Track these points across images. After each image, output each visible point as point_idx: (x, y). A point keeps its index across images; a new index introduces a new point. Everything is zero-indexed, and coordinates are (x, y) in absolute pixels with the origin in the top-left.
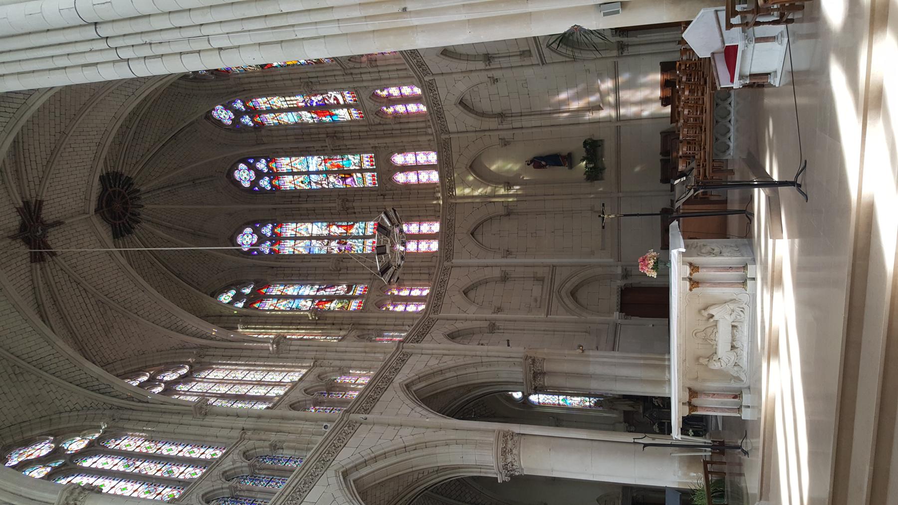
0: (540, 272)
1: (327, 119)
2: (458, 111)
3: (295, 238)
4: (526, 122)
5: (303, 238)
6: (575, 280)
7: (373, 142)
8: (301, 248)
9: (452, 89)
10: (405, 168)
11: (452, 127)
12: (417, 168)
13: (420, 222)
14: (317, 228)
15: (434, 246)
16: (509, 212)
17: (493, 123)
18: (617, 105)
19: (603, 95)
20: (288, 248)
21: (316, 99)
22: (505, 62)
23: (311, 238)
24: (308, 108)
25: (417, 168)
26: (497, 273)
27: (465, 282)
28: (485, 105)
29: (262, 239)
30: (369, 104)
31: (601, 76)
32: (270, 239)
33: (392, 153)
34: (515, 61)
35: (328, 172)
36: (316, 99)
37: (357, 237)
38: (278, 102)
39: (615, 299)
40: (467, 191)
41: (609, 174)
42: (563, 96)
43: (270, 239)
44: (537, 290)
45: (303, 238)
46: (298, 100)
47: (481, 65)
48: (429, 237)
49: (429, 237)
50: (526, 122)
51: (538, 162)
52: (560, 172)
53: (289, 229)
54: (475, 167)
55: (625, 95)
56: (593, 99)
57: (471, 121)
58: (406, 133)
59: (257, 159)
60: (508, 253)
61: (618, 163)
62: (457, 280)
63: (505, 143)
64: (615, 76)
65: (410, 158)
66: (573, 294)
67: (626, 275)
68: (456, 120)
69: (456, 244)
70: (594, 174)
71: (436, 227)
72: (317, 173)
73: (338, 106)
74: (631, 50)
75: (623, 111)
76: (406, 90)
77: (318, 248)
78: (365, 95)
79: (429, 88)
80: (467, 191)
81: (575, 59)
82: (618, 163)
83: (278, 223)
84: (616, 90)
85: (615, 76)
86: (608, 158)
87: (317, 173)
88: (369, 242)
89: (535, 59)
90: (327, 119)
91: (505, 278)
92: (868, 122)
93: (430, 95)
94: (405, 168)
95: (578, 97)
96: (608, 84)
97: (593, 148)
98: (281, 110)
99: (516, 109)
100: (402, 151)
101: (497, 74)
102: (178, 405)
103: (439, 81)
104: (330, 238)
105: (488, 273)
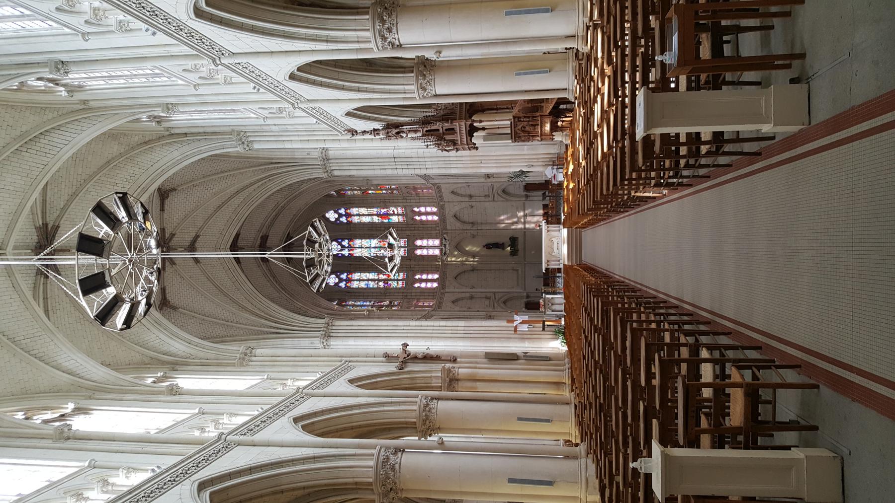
0: (489, 295)
1: (386, 221)
2: (453, 220)
3: (360, 280)
4: (484, 227)
5: (364, 280)
6: (506, 298)
7: (408, 233)
8: (363, 285)
9: (451, 210)
10: (421, 247)
11: (449, 227)
12: (428, 247)
13: (428, 274)
14: (371, 276)
15: (435, 285)
16: (473, 269)
17: (469, 227)
18: (524, 223)
19: (519, 218)
20: (355, 285)
21: (383, 211)
22: (478, 199)
23: (368, 280)
24: (378, 215)
25: (428, 247)
26: (468, 295)
27: (453, 298)
28: (465, 218)
29: (341, 280)
30: (409, 214)
31: (518, 210)
32: (345, 280)
33: (417, 239)
34: (483, 199)
35: (381, 247)
36: (383, 211)
37: (394, 280)
38: (363, 211)
39: (523, 305)
40: (453, 259)
41: (521, 253)
42: (502, 218)
43: (345, 280)
44: (487, 302)
45: (364, 280)
46: (374, 211)
47: (467, 199)
48: (432, 281)
49: (432, 281)
50: (484, 227)
51: (488, 246)
52: (498, 251)
53: (356, 276)
54: (458, 247)
55: (529, 219)
56: (515, 220)
57: (459, 225)
58: (426, 230)
59: (343, 240)
60: (473, 287)
61: (524, 248)
62: (448, 298)
63: (474, 236)
64: (524, 210)
65: (425, 242)
66: (504, 303)
67: (528, 297)
68: (451, 224)
69: (447, 283)
70: (514, 253)
71: (436, 276)
72: (375, 247)
73: (394, 214)
74: (531, 198)
75: (527, 226)
76: (429, 209)
77: (372, 284)
78: (409, 210)
79: (441, 208)
80: (453, 259)
81: (507, 200)
82: (524, 248)
83: (350, 272)
84: (525, 216)
85: (524, 210)
86: (520, 246)
87: (375, 247)
88: (400, 283)
89: (490, 199)
90: (386, 221)
91: (472, 298)
92: (800, 390)
93: (441, 213)
94: (421, 247)
95: (508, 219)
96: (521, 214)
97: (514, 241)
98: (364, 215)
99: (479, 221)
100: (422, 238)
101: (473, 204)
102: (134, 491)
103: (447, 205)
104: (379, 280)
105: (463, 295)
